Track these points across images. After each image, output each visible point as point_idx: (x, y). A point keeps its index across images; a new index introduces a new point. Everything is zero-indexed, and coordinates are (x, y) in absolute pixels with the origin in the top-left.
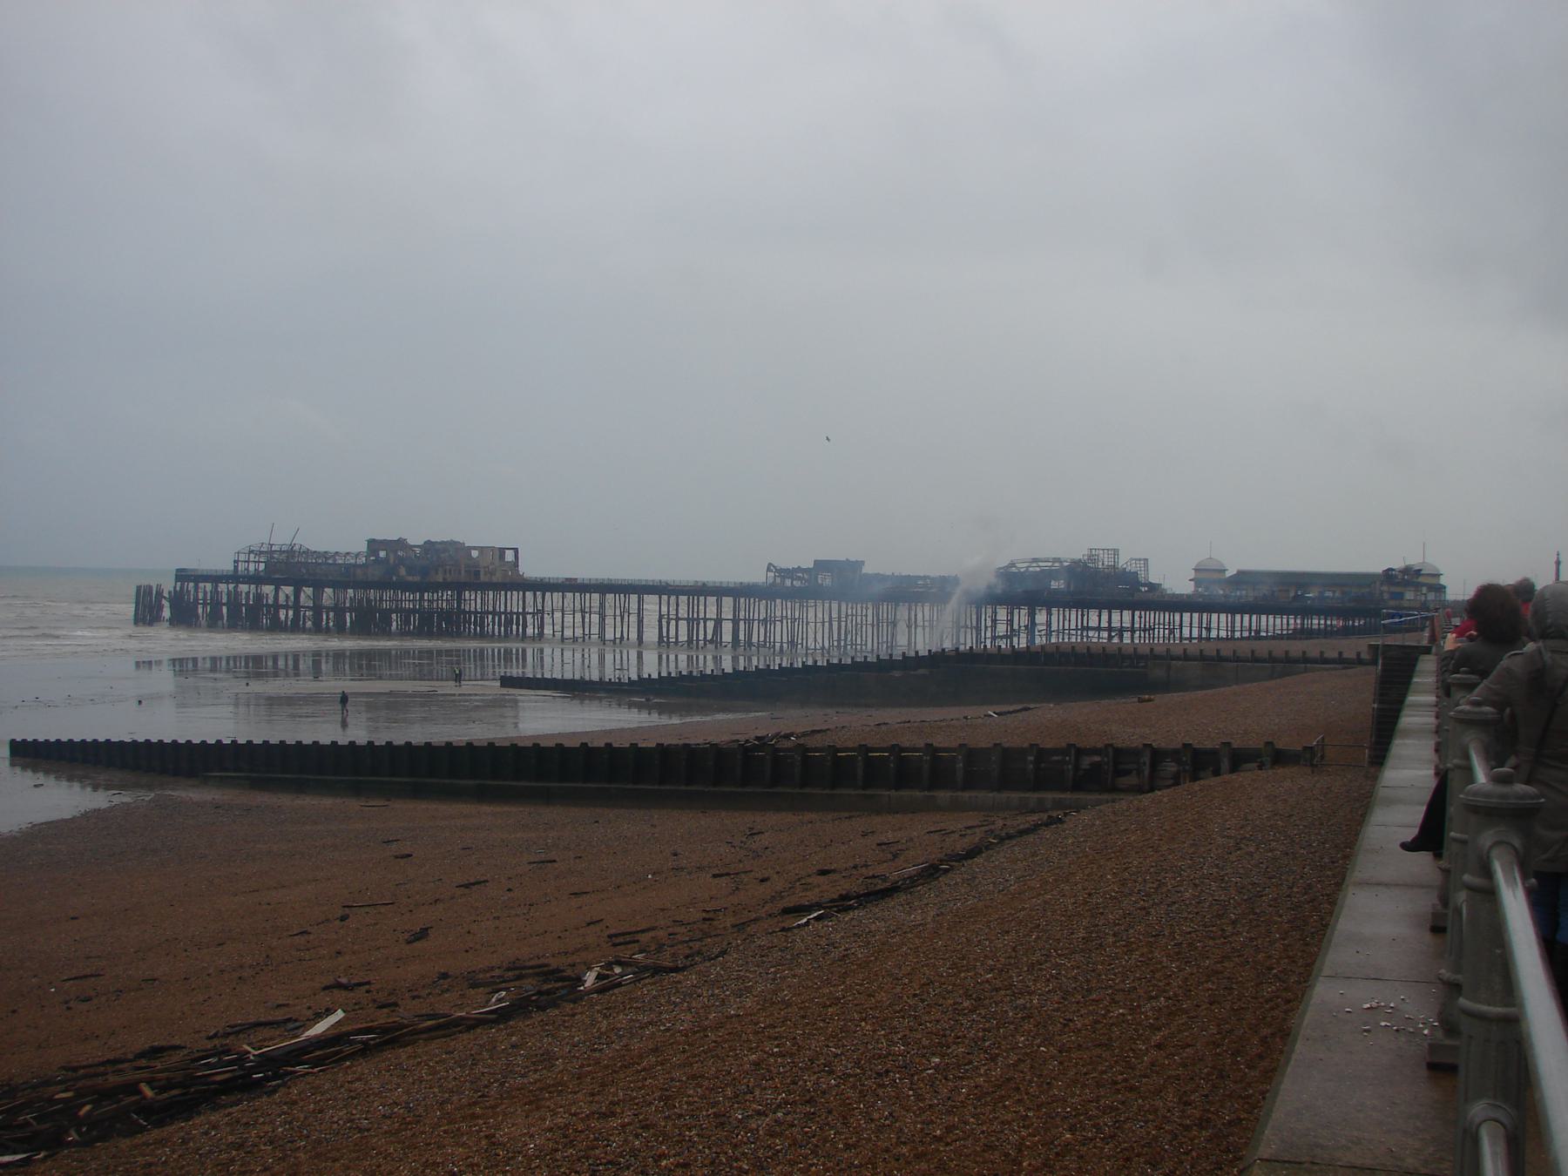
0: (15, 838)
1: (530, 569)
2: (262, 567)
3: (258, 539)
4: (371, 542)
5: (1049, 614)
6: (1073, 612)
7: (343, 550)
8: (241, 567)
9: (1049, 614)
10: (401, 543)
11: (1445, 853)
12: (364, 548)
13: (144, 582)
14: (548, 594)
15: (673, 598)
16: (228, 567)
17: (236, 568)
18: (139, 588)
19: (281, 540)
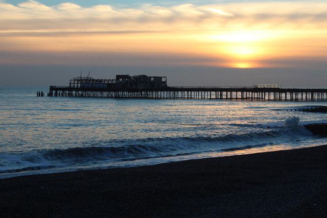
0: (95, 171)
1: (169, 84)
2: (79, 85)
3: (77, 76)
4: (117, 76)
5: (306, 94)
6: (251, 93)
7: (107, 79)
8: (72, 85)
9: (306, 94)
10: (127, 76)
11: (304, 127)
12: (115, 78)
13: (38, 91)
14: (192, 92)
15: (190, 92)
16: (68, 85)
17: (70, 85)
18: (51, 87)
19: (84, 76)
